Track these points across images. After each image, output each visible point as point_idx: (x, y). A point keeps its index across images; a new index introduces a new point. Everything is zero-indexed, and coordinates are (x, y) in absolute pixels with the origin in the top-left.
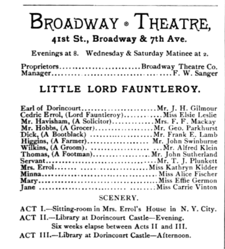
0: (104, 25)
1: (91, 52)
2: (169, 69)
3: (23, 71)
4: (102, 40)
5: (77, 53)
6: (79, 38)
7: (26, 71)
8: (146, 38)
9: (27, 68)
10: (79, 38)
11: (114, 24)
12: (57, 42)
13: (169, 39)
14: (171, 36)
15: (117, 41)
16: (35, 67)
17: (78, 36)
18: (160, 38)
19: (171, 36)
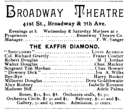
0: (53, 14)
3: (6, 38)
4: (54, 24)
5: (37, 32)
6: (40, 23)
7: (8, 38)
9: (8, 36)
10: (40, 23)
11: (60, 13)
12: (26, 26)
13: (96, 24)
14: (96, 22)
15: (63, 25)
17: (39, 22)
18: (90, 23)
19: (96, 22)
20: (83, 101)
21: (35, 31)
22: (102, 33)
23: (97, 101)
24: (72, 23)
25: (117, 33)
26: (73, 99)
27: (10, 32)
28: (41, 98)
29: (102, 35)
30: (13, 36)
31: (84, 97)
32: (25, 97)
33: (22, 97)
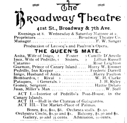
1: (51, 33)
2: (79, 30)
4: (64, 29)
6: (52, 28)
7: (17, 40)
8: (89, 28)
10: (52, 28)
13: (102, 28)
16: (22, 38)
18: (97, 28)
20: (84, 116)
21: (43, 34)
22: (102, 35)
23: (98, 116)
24: (81, 28)
25: (115, 36)
26: (76, 114)
27: (19, 34)
28: (48, 113)
29: (101, 37)
30: (21, 38)
31: (84, 112)
32: (32, 112)
33: (30, 112)
